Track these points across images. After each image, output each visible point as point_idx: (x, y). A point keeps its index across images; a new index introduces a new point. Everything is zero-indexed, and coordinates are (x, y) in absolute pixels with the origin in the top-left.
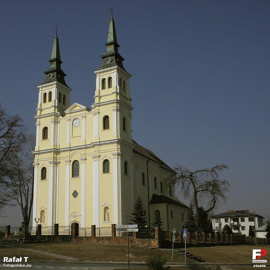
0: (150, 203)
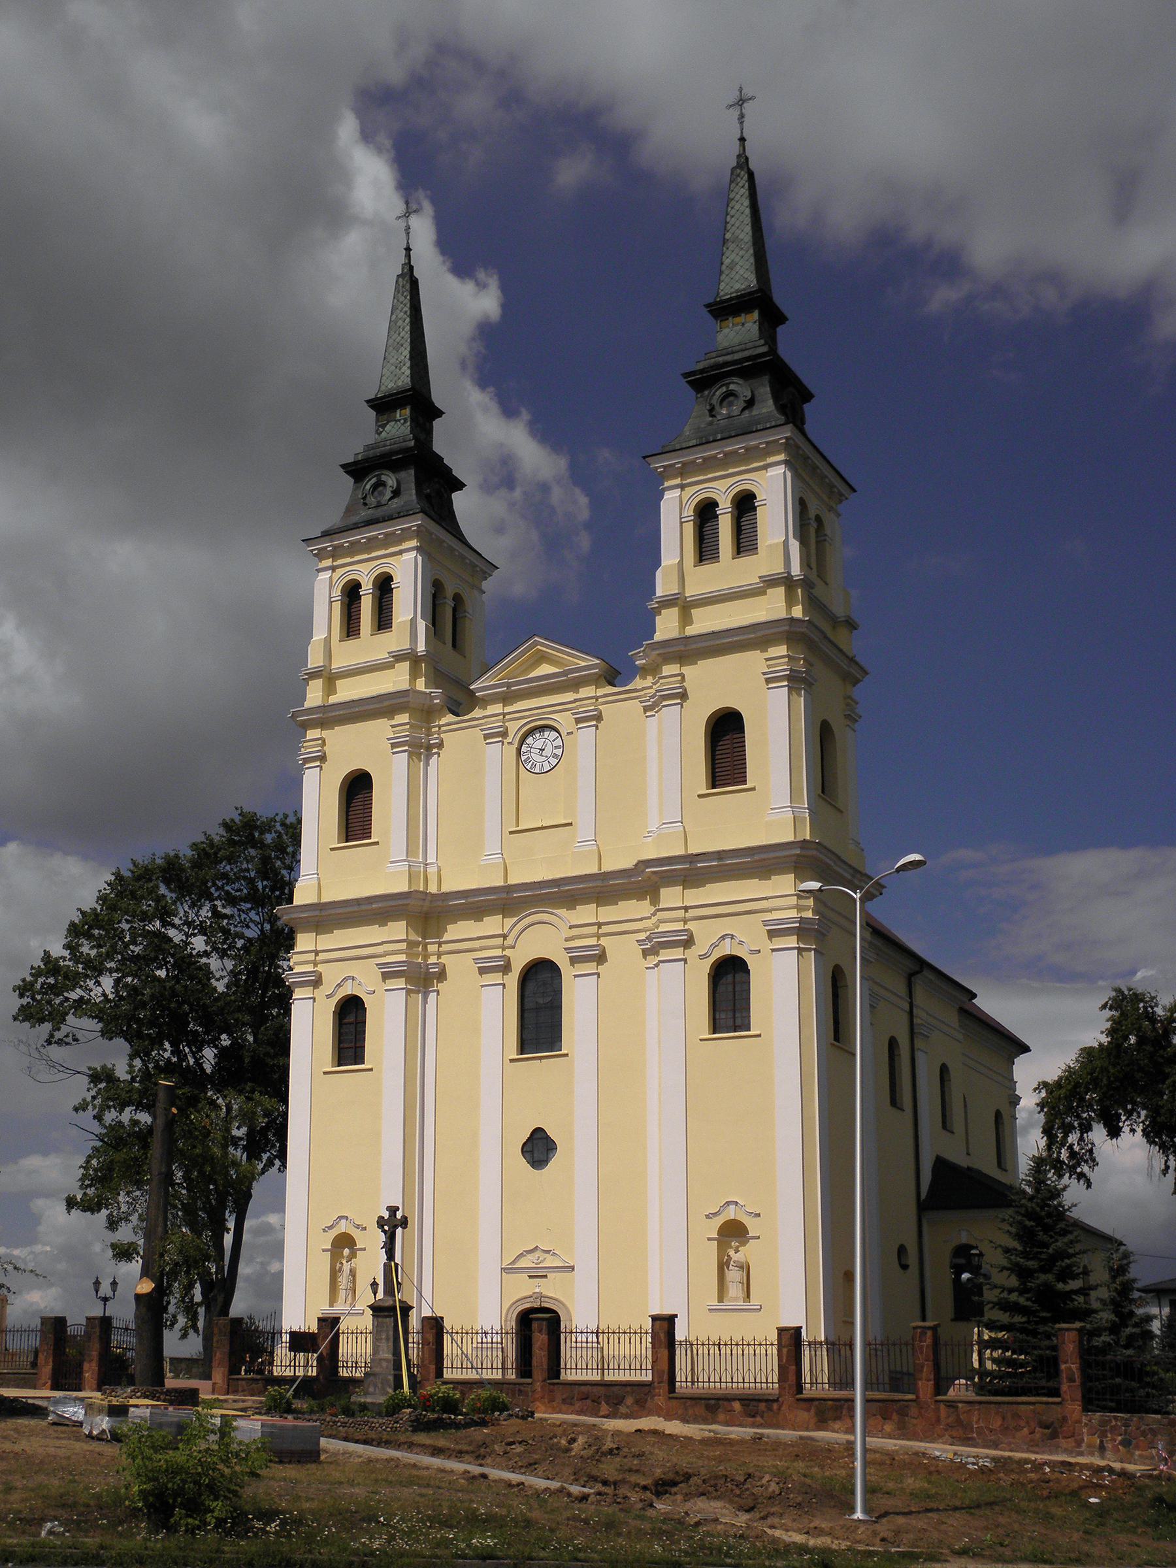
0: (923, 1207)
